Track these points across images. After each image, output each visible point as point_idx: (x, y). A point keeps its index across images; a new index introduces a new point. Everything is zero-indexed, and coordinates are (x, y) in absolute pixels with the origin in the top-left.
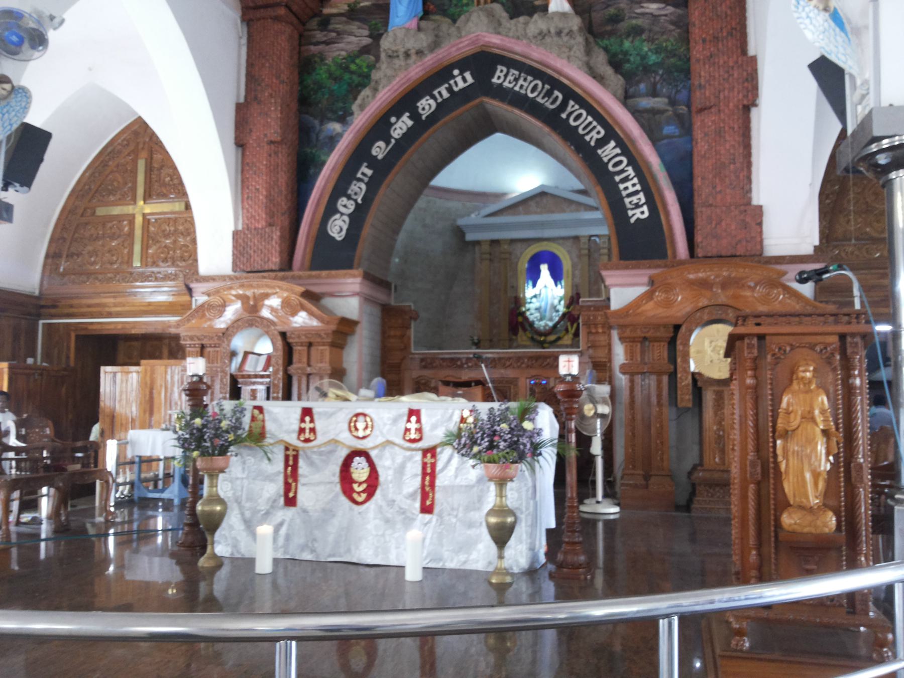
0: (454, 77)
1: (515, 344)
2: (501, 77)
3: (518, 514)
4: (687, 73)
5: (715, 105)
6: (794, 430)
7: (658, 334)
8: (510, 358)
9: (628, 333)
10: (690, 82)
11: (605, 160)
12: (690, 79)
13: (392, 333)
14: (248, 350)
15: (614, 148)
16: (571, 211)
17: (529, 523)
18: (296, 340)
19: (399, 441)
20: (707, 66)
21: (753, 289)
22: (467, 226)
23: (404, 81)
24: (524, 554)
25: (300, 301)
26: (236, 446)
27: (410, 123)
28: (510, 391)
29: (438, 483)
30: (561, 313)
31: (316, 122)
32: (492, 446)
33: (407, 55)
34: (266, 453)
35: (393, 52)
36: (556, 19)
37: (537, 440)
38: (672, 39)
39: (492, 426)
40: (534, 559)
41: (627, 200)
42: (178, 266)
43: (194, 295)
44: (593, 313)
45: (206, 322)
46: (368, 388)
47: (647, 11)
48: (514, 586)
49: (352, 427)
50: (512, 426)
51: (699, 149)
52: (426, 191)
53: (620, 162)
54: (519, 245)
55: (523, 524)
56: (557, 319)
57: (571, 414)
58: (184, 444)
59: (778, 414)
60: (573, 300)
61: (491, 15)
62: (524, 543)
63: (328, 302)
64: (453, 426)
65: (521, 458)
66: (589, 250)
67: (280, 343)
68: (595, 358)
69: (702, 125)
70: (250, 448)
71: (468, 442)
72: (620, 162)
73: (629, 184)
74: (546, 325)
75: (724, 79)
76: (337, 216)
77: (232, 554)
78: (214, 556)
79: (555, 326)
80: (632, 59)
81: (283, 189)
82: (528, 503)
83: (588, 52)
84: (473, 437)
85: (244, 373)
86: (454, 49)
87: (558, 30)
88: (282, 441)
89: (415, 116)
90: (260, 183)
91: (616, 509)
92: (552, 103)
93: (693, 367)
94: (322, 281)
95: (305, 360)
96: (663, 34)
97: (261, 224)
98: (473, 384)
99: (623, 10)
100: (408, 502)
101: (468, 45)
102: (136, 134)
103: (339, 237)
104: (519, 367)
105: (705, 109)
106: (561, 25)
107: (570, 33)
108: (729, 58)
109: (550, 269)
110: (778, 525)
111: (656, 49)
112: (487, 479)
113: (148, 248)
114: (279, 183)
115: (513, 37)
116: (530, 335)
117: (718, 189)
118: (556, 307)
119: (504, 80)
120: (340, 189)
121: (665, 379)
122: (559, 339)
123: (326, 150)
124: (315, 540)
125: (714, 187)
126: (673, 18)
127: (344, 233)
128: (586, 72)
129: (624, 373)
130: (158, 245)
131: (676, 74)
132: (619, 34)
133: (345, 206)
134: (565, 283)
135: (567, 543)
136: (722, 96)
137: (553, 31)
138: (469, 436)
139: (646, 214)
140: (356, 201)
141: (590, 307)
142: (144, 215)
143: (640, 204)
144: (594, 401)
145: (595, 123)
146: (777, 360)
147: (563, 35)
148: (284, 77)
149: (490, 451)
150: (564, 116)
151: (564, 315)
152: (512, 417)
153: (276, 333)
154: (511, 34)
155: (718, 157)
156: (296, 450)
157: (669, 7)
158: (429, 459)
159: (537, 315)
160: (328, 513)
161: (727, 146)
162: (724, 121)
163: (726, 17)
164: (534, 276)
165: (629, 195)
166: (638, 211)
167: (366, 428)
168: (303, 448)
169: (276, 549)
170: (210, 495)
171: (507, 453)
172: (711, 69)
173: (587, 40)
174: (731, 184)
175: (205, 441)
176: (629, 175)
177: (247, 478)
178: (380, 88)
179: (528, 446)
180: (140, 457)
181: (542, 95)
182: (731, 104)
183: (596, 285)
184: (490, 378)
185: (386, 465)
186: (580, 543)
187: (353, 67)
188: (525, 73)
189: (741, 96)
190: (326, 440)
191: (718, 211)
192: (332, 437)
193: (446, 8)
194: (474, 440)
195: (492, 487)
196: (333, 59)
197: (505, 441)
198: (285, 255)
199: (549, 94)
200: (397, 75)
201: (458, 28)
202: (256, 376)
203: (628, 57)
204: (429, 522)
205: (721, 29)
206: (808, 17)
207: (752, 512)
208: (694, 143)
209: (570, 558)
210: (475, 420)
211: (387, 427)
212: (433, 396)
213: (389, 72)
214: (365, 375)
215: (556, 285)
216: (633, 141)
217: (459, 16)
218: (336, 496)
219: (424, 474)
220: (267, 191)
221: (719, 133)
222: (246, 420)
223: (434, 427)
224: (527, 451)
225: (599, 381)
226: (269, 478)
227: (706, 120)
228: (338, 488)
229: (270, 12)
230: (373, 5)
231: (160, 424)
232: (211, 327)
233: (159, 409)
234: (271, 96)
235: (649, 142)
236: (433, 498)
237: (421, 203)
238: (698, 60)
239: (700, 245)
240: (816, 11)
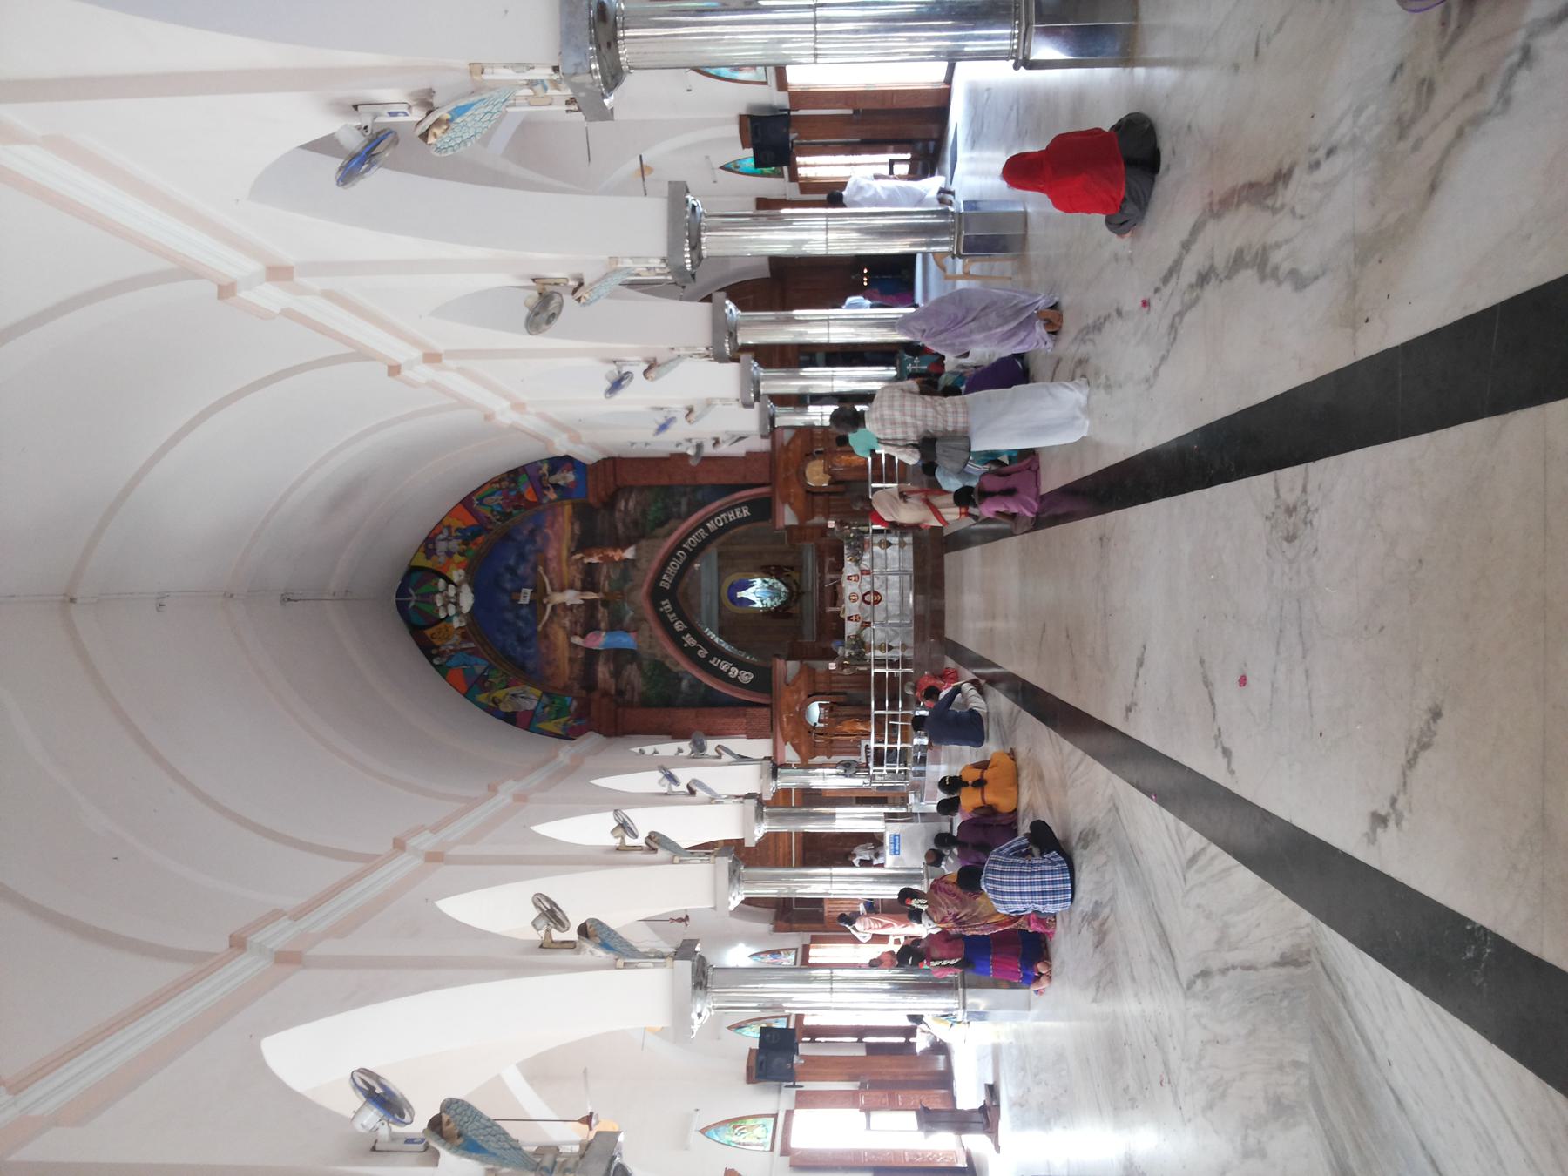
0: (664, 611)
2: (666, 582)
11: (716, 528)
49: (855, 601)
83: (656, 537)
89: (684, 633)
120: (723, 676)
121: (832, 497)
122: (795, 581)
127: (749, 673)
150: (691, 550)
151: (777, 578)
156: (863, 622)
159: (776, 600)
185: (867, 588)
187: (649, 674)
199: (678, 558)
223: (853, 571)
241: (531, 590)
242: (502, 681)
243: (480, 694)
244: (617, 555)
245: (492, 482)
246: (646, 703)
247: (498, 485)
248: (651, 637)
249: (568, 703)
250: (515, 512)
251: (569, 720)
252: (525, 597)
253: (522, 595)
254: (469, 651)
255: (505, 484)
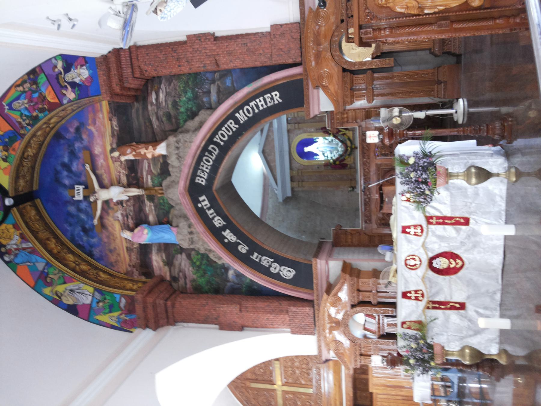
1: (353, 165)
2: (202, 181)
3: (469, 165)
4: (196, 75)
5: (214, 58)
6: (418, 3)
7: (348, 81)
8: (364, 170)
9: (349, 100)
10: (202, 73)
11: (246, 118)
12: (200, 73)
13: (350, 240)
14: (362, 328)
15: (239, 114)
16: (273, 135)
17: (474, 157)
18: (356, 299)
19: (422, 239)
20: (193, 63)
21: (320, 26)
22: (283, 196)
23: (205, 234)
24: (495, 160)
25: (332, 296)
26: (427, 338)
27: (228, 231)
28: (383, 169)
29: (449, 215)
30: (333, 138)
31: (229, 284)
32: (425, 182)
33: (191, 233)
34: (432, 321)
35: (190, 241)
36: (170, 150)
37: (421, 155)
38: (179, 84)
39: (412, 182)
40: (497, 153)
41: (269, 105)
42: (312, 367)
43: (329, 358)
44: (335, 120)
45: (345, 352)
46: (384, 256)
47: (164, 99)
48: (516, 166)
49: (413, 268)
50: (412, 170)
51: (239, 64)
52: (263, 220)
53: (248, 110)
54: (293, 165)
55: (476, 161)
56: (337, 141)
57: (404, 134)
58: (425, 371)
59: (408, 13)
60: (325, 132)
61: (169, 187)
62: (488, 160)
63: (332, 280)
64: (412, 206)
65: (432, 164)
66: (295, 123)
67: (358, 309)
68: (363, 118)
69: (226, 63)
70: (428, 331)
71: (423, 197)
72: (248, 110)
73: (260, 104)
74: (341, 146)
75: (200, 53)
76: (281, 273)
77: (496, 343)
78: (499, 354)
79: (341, 141)
80: (190, 106)
81: (266, 304)
82: (462, 159)
83: (187, 131)
84: (419, 194)
85: (377, 330)
86: (187, 206)
87: (176, 149)
88: (423, 311)
89: (224, 228)
90: (264, 318)
91: (461, 100)
92: (215, 150)
93: (369, 59)
94: (320, 282)
95: (368, 294)
96: (176, 89)
97: (286, 317)
98: (381, 192)
99: (164, 113)
100: (462, 233)
101: (185, 199)
102: (237, 387)
103: (293, 272)
104: (369, 163)
105: (217, 63)
106: (173, 147)
107: (177, 142)
108: (188, 51)
109: (307, 146)
110: (479, 8)
111: (184, 93)
112: (446, 185)
113: (301, 384)
114: (263, 306)
115: (180, 174)
116: (347, 156)
117: (261, 52)
118: (330, 142)
119: (203, 178)
120: (265, 271)
121: (376, 75)
122: (349, 139)
123: (243, 279)
124: (487, 292)
125: (261, 54)
126: (167, 85)
127: (290, 269)
128: (198, 132)
129: (373, 100)
130: (300, 378)
131: (197, 81)
132: (177, 114)
133: (275, 268)
134: (315, 137)
135: (488, 133)
136: (209, 54)
137: (177, 152)
138: (419, 197)
139: (277, 93)
140: (272, 262)
141: (331, 122)
142: (283, 385)
143: (270, 96)
144: (391, 118)
145: (226, 126)
146: (374, 17)
147: (178, 146)
148: (204, 302)
149: (428, 183)
150: (222, 143)
151: (335, 136)
152: (406, 171)
153: (352, 311)
154: (178, 175)
155: (243, 53)
157: (162, 87)
158: (434, 221)
159: (334, 152)
160: (469, 283)
161: (237, 48)
162: (223, 52)
163: (166, 54)
164: (311, 155)
165: (266, 103)
166: (275, 98)
167: (413, 259)
168: (428, 298)
169: (493, 316)
170: (459, 356)
171: (430, 173)
172: (195, 61)
173: (181, 132)
174: (259, 45)
175: (424, 357)
176: (255, 104)
177: (447, 332)
178: (209, 248)
179: (425, 160)
180: (432, 396)
181: (211, 156)
182: (214, 48)
183: (319, 119)
184: (376, 182)
186: (487, 125)
188: (199, 166)
189: (209, 43)
190: (422, 284)
191: (274, 51)
192: (421, 281)
193: (165, 212)
194: (421, 194)
195: (453, 181)
196: (194, 274)
197: (422, 174)
198: (305, 304)
200: (202, 239)
201: (177, 204)
202: (379, 323)
203: (189, 109)
204: (475, 220)
205: (172, 56)
206: (170, 11)
207: (471, 25)
208: (235, 68)
209: (497, 131)
210: (408, 193)
211: (413, 246)
212: (392, 218)
213: (201, 243)
214: (376, 257)
215: (317, 142)
216: (236, 103)
217: (169, 204)
218: (458, 278)
219: (444, 223)
220: (268, 314)
221: (230, 54)
222: (411, 332)
223: (413, 217)
224: (428, 161)
225: (378, 115)
226: (447, 319)
227: (223, 62)
228: (453, 277)
229: (170, 310)
230: (165, 252)
231: (409, 383)
232: (349, 349)
233: (399, 382)
234: (215, 310)
235: (236, 94)
236: (459, 218)
237: (270, 223)
238: (190, 69)
239: (294, 60)
240: (167, 7)
241: (83, 187)
242: (60, 278)
243: (45, 288)
244: (149, 152)
245: (16, 85)
246: (198, 290)
247: (21, 88)
248: (191, 233)
249: (118, 300)
250: (41, 115)
251: (121, 314)
252: (78, 193)
253: (76, 192)
254: (29, 250)
255: (27, 86)
